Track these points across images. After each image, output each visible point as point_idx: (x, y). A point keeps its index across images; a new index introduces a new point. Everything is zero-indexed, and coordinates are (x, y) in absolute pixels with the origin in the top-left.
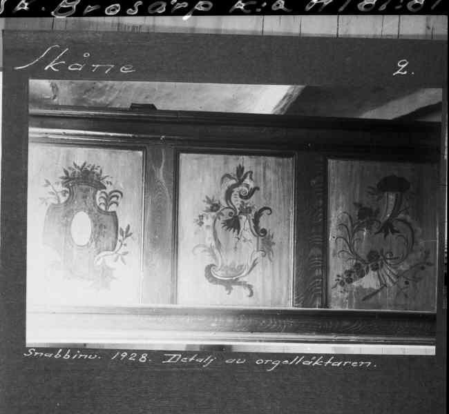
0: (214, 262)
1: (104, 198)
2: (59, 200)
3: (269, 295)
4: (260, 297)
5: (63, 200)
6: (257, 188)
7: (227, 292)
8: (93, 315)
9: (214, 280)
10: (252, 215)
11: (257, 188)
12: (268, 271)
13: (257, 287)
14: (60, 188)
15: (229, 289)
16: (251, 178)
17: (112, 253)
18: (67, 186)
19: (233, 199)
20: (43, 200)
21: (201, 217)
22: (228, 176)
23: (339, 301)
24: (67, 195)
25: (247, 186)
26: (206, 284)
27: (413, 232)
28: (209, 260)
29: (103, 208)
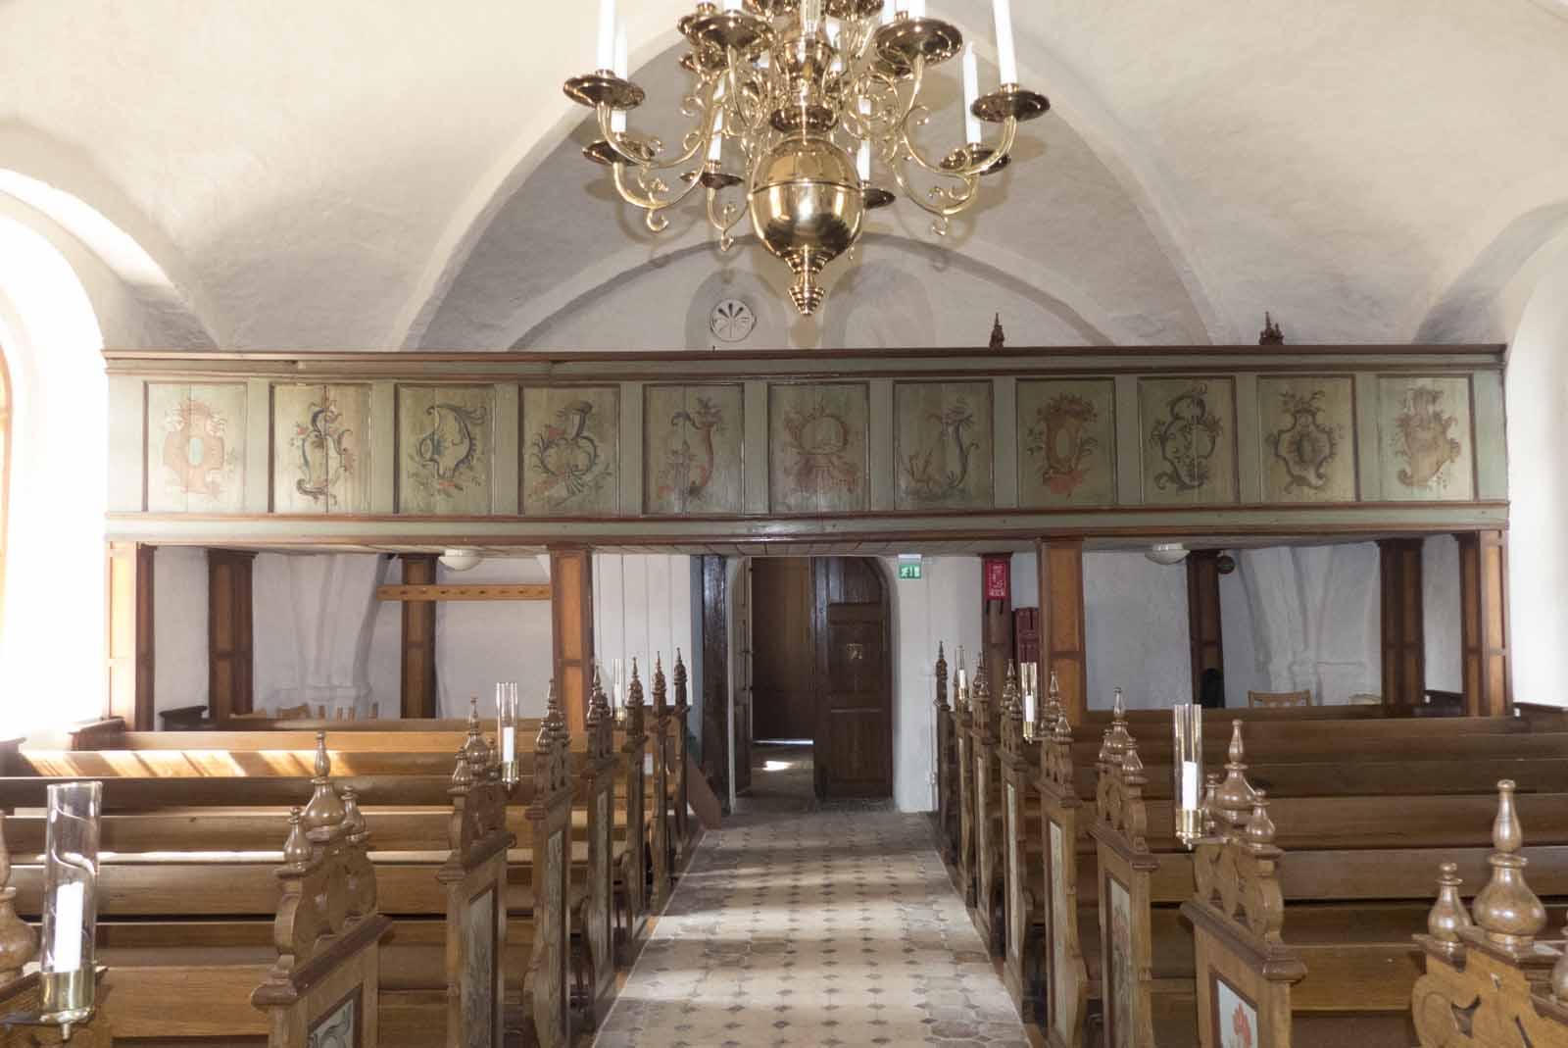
0: (303, 478)
1: (471, 413)
2: (175, 428)
3: (350, 505)
4: (342, 504)
5: (179, 428)
6: (340, 414)
7: (1428, 490)
8: (575, 513)
9: (306, 492)
10: (336, 437)
11: (340, 414)
12: (349, 485)
13: (340, 498)
14: (177, 418)
15: (316, 498)
16: (335, 405)
17: (1223, 441)
18: (183, 416)
19: (318, 424)
20: (163, 428)
21: (292, 439)
22: (314, 405)
23: (533, 506)
24: (183, 424)
25: (332, 412)
26: (297, 495)
27: (595, 447)
28: (299, 476)
29: (212, 433)
